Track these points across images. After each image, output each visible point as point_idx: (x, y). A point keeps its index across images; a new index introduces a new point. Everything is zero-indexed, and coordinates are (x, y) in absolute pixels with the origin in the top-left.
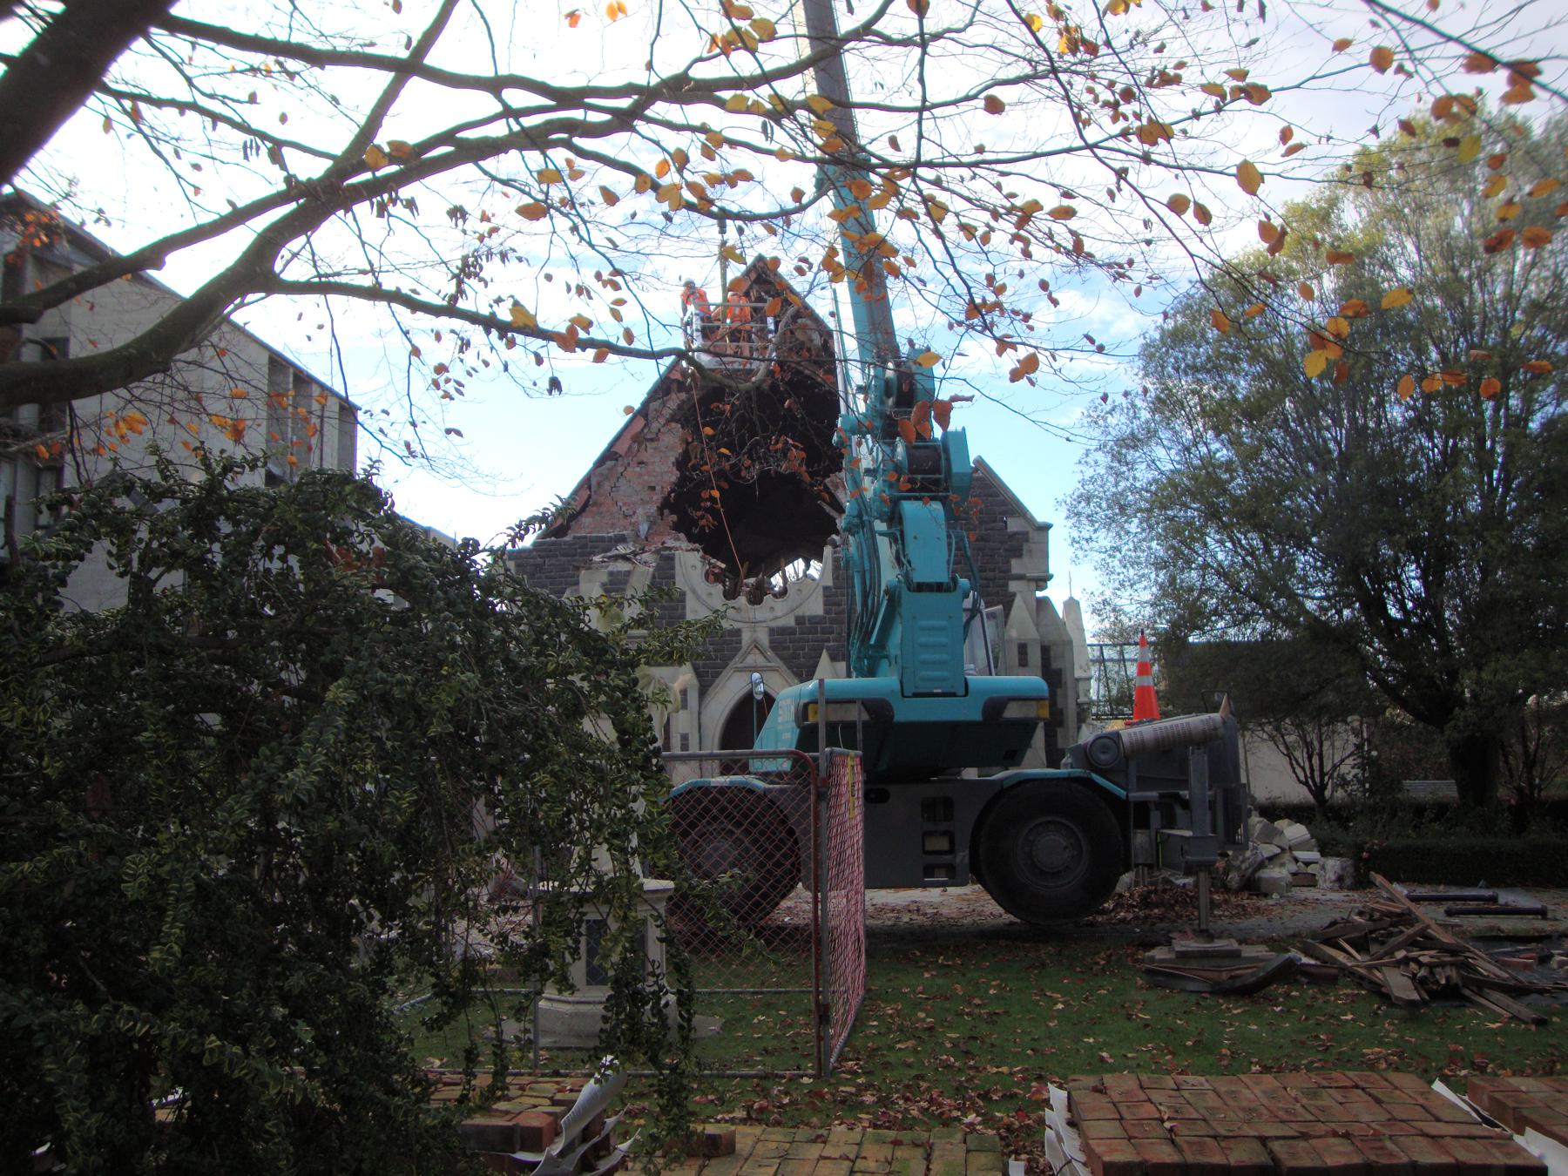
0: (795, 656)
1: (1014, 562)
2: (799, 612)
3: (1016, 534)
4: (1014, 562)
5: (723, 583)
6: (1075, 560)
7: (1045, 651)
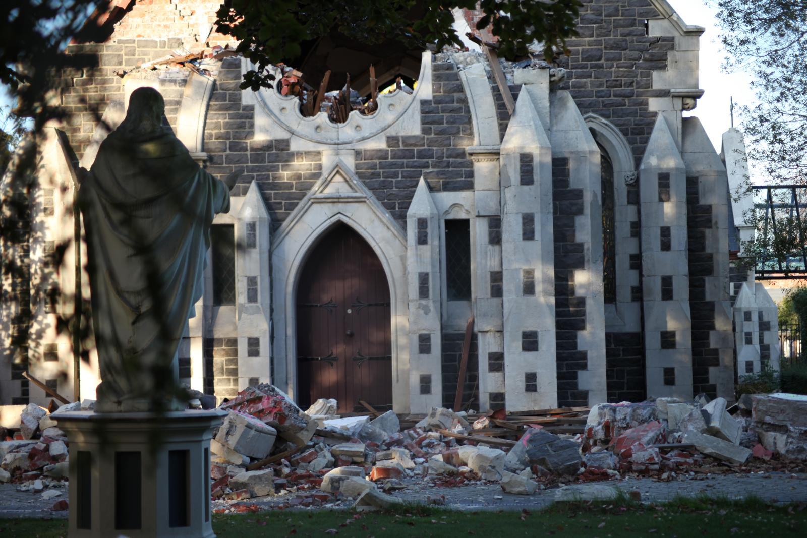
0: (384, 185)
1: (655, 74)
2: (392, 132)
3: (658, 40)
4: (655, 74)
5: (300, 95)
6: (727, 67)
7: (692, 183)
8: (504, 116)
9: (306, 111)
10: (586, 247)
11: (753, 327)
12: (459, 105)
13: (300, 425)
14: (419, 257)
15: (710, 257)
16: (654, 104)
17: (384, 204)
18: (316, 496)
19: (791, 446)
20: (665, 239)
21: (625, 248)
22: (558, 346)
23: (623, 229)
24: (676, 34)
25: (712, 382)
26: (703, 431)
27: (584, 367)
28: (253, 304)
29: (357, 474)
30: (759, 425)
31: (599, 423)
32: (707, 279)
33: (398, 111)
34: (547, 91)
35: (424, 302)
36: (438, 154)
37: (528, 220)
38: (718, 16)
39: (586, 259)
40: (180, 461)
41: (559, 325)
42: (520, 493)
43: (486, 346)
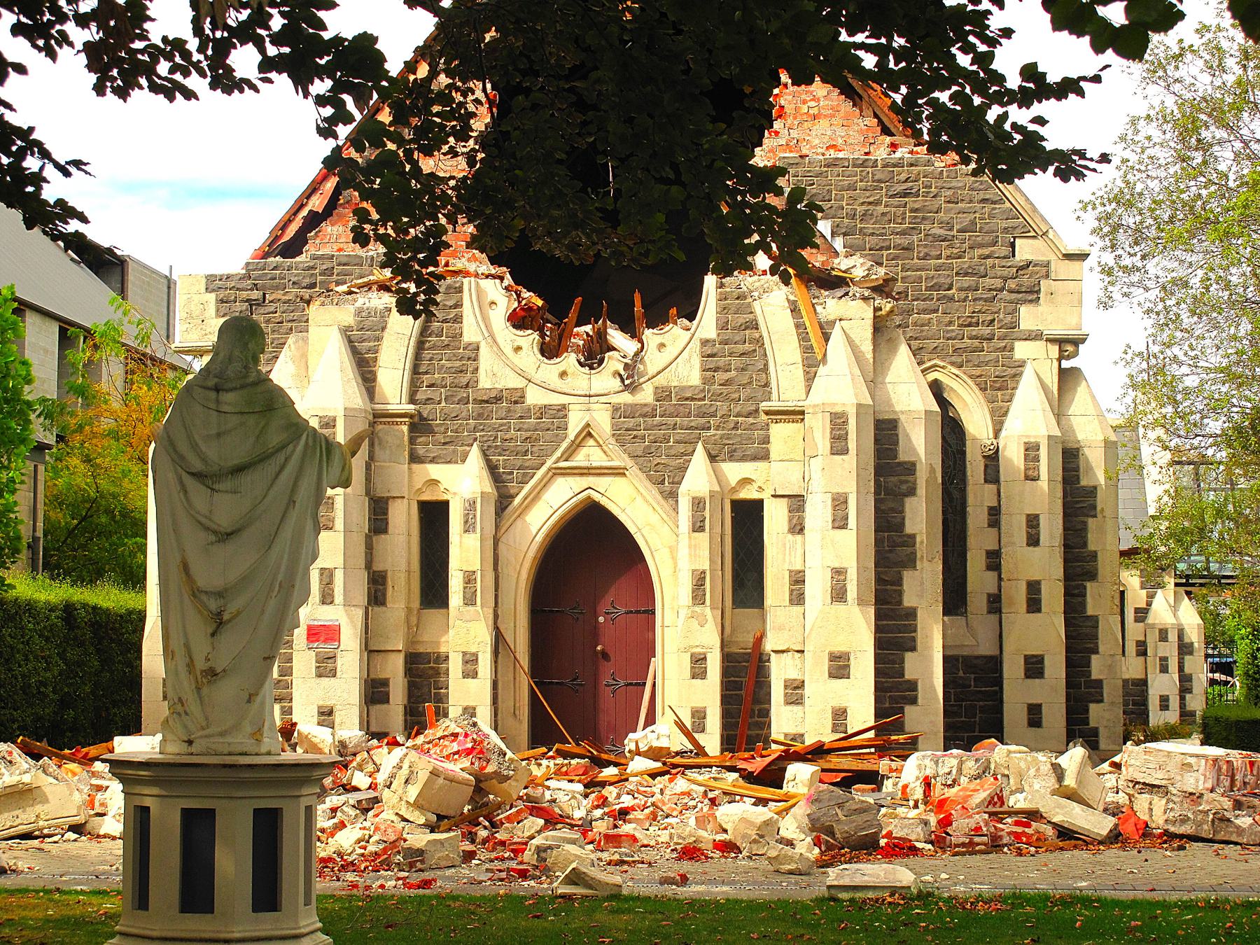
1: (1024, 310)
4: (1024, 310)
8: (812, 363)
9: (550, 351)
10: (918, 539)
11: (1170, 650)
12: (752, 347)
13: (505, 773)
14: (693, 547)
15: (1094, 555)
16: (1022, 350)
17: (649, 478)
18: (513, 870)
19: (1172, 814)
20: (1033, 531)
21: (978, 541)
22: (878, 673)
23: (976, 517)
24: (1052, 257)
25: (1092, 724)
26: (1054, 793)
27: (913, 701)
28: (470, 608)
29: (573, 842)
30: (1131, 785)
31: (918, 778)
32: (1088, 585)
33: (673, 353)
34: (870, 330)
35: (698, 609)
36: (733, 411)
37: (839, 502)
38: (1094, 232)
39: (919, 556)
40: (268, 827)
41: (880, 644)
42: (791, 872)
43: (780, 672)
